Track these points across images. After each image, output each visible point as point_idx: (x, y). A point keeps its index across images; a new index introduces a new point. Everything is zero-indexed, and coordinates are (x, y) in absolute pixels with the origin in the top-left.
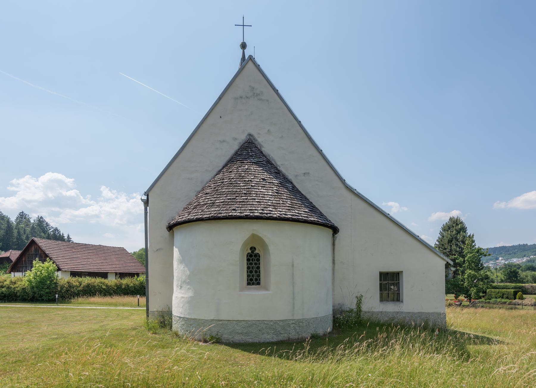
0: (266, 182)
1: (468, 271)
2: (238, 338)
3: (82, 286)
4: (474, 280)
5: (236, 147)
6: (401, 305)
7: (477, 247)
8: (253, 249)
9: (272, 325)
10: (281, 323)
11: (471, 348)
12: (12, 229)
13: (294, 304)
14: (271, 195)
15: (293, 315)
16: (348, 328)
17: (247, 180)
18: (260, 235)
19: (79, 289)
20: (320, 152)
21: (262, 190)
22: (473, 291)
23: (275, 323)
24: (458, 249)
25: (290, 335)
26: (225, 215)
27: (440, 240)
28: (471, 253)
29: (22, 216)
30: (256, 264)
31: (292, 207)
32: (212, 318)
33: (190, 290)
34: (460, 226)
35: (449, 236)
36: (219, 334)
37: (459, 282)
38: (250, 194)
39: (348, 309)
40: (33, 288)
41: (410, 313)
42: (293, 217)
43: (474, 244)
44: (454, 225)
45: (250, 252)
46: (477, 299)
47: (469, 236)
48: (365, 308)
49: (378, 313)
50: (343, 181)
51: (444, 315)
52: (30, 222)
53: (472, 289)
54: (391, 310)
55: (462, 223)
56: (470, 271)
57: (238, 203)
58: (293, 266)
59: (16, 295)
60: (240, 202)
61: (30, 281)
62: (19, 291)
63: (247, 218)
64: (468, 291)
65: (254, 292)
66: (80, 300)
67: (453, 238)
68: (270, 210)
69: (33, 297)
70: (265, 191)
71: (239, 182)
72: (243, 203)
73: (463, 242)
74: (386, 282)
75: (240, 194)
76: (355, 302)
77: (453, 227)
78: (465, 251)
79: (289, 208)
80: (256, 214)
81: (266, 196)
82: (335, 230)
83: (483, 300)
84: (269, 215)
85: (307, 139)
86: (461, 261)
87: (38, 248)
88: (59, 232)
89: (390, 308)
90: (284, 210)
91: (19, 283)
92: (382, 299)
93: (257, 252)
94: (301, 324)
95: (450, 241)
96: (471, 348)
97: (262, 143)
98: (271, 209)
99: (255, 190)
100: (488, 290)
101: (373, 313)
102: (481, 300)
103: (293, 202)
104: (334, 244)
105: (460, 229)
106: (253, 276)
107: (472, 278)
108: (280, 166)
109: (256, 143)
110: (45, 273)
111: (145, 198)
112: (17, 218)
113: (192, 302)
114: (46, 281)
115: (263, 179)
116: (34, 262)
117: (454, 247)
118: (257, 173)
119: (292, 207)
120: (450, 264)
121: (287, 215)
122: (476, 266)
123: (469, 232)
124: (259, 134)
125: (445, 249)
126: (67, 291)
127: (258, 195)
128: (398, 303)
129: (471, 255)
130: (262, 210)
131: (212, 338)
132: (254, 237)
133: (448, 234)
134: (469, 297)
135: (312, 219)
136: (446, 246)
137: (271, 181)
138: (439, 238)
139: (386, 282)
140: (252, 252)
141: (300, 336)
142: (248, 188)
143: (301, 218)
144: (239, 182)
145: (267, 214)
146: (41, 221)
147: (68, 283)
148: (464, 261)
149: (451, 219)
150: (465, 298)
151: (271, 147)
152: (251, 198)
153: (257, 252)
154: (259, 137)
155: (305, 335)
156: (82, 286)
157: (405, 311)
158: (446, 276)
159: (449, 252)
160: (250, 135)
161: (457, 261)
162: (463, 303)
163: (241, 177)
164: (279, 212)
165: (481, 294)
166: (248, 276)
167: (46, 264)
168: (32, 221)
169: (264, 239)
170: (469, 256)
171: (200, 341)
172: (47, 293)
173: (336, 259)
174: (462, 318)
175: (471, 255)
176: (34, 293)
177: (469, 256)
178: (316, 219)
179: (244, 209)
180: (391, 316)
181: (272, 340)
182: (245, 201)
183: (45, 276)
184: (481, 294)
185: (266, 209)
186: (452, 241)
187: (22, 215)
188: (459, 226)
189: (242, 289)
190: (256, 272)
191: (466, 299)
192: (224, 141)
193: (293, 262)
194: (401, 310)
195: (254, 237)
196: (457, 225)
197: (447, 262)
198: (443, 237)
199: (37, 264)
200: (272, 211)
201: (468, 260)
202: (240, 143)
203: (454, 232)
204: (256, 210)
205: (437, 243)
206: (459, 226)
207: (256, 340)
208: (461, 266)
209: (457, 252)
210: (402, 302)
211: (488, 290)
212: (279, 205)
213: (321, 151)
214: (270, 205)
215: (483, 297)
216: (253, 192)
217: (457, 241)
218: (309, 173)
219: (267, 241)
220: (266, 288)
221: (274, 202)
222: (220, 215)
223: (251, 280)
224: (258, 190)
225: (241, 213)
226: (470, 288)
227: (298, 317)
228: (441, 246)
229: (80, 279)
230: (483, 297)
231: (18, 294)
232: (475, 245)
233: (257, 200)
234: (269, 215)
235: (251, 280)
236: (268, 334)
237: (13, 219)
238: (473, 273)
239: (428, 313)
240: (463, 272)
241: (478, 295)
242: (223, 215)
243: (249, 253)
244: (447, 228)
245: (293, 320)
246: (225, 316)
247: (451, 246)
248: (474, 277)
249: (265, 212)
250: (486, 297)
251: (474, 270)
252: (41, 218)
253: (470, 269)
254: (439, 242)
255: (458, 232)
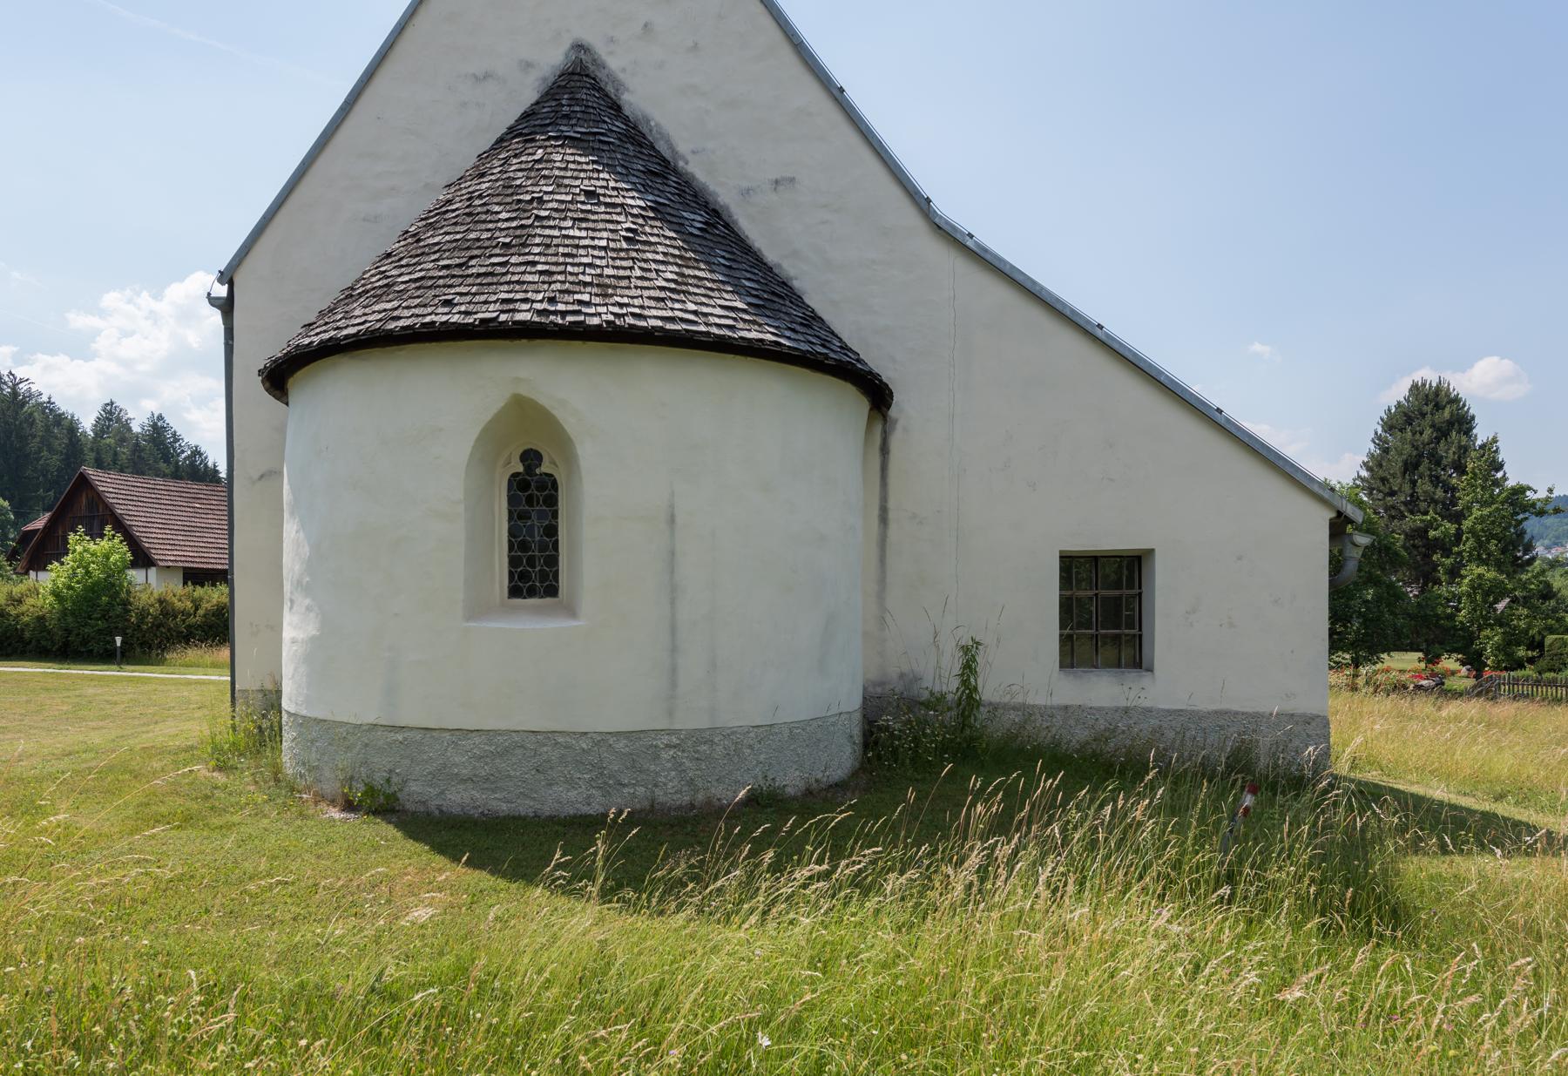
0: (599, 204)
1: (1474, 570)
2: (458, 798)
3: (201, 612)
4: (1496, 601)
5: (527, 94)
6: (1145, 680)
7: (1510, 483)
8: (531, 458)
9: (588, 752)
10: (621, 745)
11: (1419, 870)
12: (81, 452)
13: (674, 670)
14: (604, 248)
15: (670, 714)
16: (918, 771)
17: (528, 197)
18: (543, 401)
19: (192, 620)
20: (836, 95)
21: (571, 233)
22: (1490, 640)
23: (597, 744)
24: (1439, 493)
25: (658, 792)
26: (408, 322)
27: (1375, 465)
28: (1484, 504)
29: (110, 417)
30: (541, 515)
31: (679, 288)
32: (371, 720)
33: (312, 615)
34: (1447, 411)
35: (1408, 448)
36: (395, 779)
37: (1440, 610)
38: (524, 245)
39: (925, 695)
40: (64, 612)
41: (1179, 712)
42: (669, 326)
43: (1499, 475)
44: (1428, 409)
45: (520, 469)
46: (1506, 669)
47: (1483, 447)
48: (990, 688)
49: (1049, 712)
50: (923, 205)
51: (1317, 726)
52: (130, 429)
53: (1487, 632)
54: (1105, 702)
55: (1456, 400)
56: (1481, 570)
57: (470, 281)
58: (672, 520)
59: (21, 639)
60: (479, 275)
61: (56, 594)
62: (27, 625)
63: (489, 332)
64: (1471, 638)
65: (531, 624)
66: (192, 654)
67: (1421, 456)
68: (580, 302)
69: (66, 644)
70: (584, 234)
71: (497, 208)
72: (489, 280)
73: (1460, 469)
74: (1090, 593)
75: (484, 248)
76: (957, 670)
77: (1423, 415)
78: (1464, 499)
79: (662, 295)
80: (519, 317)
81: (582, 252)
82: (878, 395)
83: (1529, 671)
84: (570, 318)
85: (786, 52)
86: (1446, 534)
87: (97, 499)
88: (204, 461)
89: (1101, 691)
90: (637, 302)
91: (30, 601)
92: (1073, 654)
93: (545, 468)
94: (704, 747)
95: (1410, 467)
96: (1419, 870)
97: (621, 76)
98: (586, 297)
99: (547, 232)
100: (1550, 639)
101: (1027, 711)
102: (1520, 673)
103: (687, 272)
104: (885, 450)
105: (1450, 423)
106: (531, 562)
107: (1487, 594)
108: (690, 157)
109: (601, 75)
110: (97, 572)
111: (222, 291)
112: (98, 420)
113: (318, 654)
114: (99, 597)
115: (590, 194)
116: (72, 537)
117: (1424, 486)
118: (572, 169)
119: (679, 288)
120: (1349, 521)
121: (644, 318)
122: (1503, 552)
123: (1481, 434)
124: (612, 40)
125: (1392, 493)
126: (158, 627)
127: (551, 251)
128: (1131, 675)
129: (1486, 511)
130: (552, 300)
131: (371, 791)
132: (524, 412)
133: (1403, 441)
134: (1475, 662)
135: (753, 335)
136: (1395, 484)
137: (618, 201)
138: (1371, 456)
139: (1090, 593)
140: (529, 469)
141: (700, 797)
142: (522, 227)
143: (702, 328)
144: (497, 208)
145: (564, 314)
146: (158, 430)
147: (161, 601)
148: (1459, 535)
149: (1415, 388)
150: (1463, 664)
151: (652, 92)
152: (521, 259)
153: (545, 468)
154: (611, 53)
155: (720, 792)
156: (201, 612)
157: (1162, 706)
158: (1336, 565)
159: (1405, 503)
160: (579, 47)
161: (1432, 533)
162: (1453, 683)
163: (509, 187)
164: (616, 310)
165: (1521, 652)
166: (513, 562)
167: (104, 544)
168: (136, 429)
169: (559, 414)
170: (1476, 513)
171: (333, 802)
172: (100, 631)
173: (891, 504)
174: (1404, 733)
175: (1486, 511)
176: (68, 631)
177: (1476, 513)
178: (769, 337)
179: (483, 298)
180: (1102, 724)
181: (585, 810)
182: (499, 270)
183: (97, 584)
184: (1521, 652)
185: (567, 298)
186: (1416, 466)
187: (110, 413)
188: (1447, 413)
189: (476, 610)
190: (524, 546)
191: (1464, 670)
192: (487, 76)
193: (672, 507)
194: (1147, 704)
195: (524, 412)
196: (1438, 407)
197: (1339, 514)
198: (1386, 451)
199: (79, 544)
200: (588, 304)
201: (1472, 531)
202: (545, 79)
203: (1428, 432)
204: (525, 300)
205: (1364, 473)
206: (1447, 413)
207: (525, 807)
208: (1447, 553)
209: (1436, 502)
210: (1150, 670)
211: (1550, 639)
212: (624, 283)
213: (842, 90)
214: (586, 284)
215: (1531, 661)
216: (537, 240)
217: (1438, 463)
218: (792, 180)
219: (570, 424)
220: (571, 611)
221: (608, 271)
222: (391, 325)
223: (524, 576)
224: (556, 233)
225: (467, 313)
226: (1480, 629)
227: (691, 719)
228: (1379, 483)
229: (199, 592)
230: (1531, 661)
231: (27, 635)
232: (1505, 478)
233: (540, 267)
234: (570, 318)
235: (524, 576)
236: (571, 783)
237: (87, 423)
238: (1491, 575)
239: (1256, 717)
240: (1454, 573)
241: (1509, 655)
242: (401, 323)
243: (515, 475)
244: (1400, 421)
245: (670, 732)
246: (413, 714)
247: (1414, 483)
248: (1497, 591)
249: (561, 307)
250: (1543, 663)
251: (1499, 566)
252: (160, 417)
253: (1482, 562)
254: (1369, 469)
255: (1442, 433)
